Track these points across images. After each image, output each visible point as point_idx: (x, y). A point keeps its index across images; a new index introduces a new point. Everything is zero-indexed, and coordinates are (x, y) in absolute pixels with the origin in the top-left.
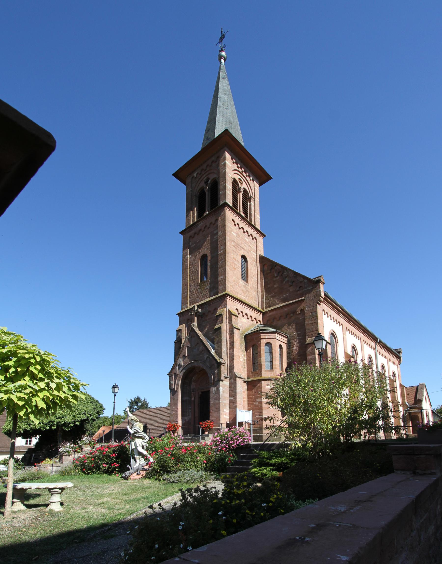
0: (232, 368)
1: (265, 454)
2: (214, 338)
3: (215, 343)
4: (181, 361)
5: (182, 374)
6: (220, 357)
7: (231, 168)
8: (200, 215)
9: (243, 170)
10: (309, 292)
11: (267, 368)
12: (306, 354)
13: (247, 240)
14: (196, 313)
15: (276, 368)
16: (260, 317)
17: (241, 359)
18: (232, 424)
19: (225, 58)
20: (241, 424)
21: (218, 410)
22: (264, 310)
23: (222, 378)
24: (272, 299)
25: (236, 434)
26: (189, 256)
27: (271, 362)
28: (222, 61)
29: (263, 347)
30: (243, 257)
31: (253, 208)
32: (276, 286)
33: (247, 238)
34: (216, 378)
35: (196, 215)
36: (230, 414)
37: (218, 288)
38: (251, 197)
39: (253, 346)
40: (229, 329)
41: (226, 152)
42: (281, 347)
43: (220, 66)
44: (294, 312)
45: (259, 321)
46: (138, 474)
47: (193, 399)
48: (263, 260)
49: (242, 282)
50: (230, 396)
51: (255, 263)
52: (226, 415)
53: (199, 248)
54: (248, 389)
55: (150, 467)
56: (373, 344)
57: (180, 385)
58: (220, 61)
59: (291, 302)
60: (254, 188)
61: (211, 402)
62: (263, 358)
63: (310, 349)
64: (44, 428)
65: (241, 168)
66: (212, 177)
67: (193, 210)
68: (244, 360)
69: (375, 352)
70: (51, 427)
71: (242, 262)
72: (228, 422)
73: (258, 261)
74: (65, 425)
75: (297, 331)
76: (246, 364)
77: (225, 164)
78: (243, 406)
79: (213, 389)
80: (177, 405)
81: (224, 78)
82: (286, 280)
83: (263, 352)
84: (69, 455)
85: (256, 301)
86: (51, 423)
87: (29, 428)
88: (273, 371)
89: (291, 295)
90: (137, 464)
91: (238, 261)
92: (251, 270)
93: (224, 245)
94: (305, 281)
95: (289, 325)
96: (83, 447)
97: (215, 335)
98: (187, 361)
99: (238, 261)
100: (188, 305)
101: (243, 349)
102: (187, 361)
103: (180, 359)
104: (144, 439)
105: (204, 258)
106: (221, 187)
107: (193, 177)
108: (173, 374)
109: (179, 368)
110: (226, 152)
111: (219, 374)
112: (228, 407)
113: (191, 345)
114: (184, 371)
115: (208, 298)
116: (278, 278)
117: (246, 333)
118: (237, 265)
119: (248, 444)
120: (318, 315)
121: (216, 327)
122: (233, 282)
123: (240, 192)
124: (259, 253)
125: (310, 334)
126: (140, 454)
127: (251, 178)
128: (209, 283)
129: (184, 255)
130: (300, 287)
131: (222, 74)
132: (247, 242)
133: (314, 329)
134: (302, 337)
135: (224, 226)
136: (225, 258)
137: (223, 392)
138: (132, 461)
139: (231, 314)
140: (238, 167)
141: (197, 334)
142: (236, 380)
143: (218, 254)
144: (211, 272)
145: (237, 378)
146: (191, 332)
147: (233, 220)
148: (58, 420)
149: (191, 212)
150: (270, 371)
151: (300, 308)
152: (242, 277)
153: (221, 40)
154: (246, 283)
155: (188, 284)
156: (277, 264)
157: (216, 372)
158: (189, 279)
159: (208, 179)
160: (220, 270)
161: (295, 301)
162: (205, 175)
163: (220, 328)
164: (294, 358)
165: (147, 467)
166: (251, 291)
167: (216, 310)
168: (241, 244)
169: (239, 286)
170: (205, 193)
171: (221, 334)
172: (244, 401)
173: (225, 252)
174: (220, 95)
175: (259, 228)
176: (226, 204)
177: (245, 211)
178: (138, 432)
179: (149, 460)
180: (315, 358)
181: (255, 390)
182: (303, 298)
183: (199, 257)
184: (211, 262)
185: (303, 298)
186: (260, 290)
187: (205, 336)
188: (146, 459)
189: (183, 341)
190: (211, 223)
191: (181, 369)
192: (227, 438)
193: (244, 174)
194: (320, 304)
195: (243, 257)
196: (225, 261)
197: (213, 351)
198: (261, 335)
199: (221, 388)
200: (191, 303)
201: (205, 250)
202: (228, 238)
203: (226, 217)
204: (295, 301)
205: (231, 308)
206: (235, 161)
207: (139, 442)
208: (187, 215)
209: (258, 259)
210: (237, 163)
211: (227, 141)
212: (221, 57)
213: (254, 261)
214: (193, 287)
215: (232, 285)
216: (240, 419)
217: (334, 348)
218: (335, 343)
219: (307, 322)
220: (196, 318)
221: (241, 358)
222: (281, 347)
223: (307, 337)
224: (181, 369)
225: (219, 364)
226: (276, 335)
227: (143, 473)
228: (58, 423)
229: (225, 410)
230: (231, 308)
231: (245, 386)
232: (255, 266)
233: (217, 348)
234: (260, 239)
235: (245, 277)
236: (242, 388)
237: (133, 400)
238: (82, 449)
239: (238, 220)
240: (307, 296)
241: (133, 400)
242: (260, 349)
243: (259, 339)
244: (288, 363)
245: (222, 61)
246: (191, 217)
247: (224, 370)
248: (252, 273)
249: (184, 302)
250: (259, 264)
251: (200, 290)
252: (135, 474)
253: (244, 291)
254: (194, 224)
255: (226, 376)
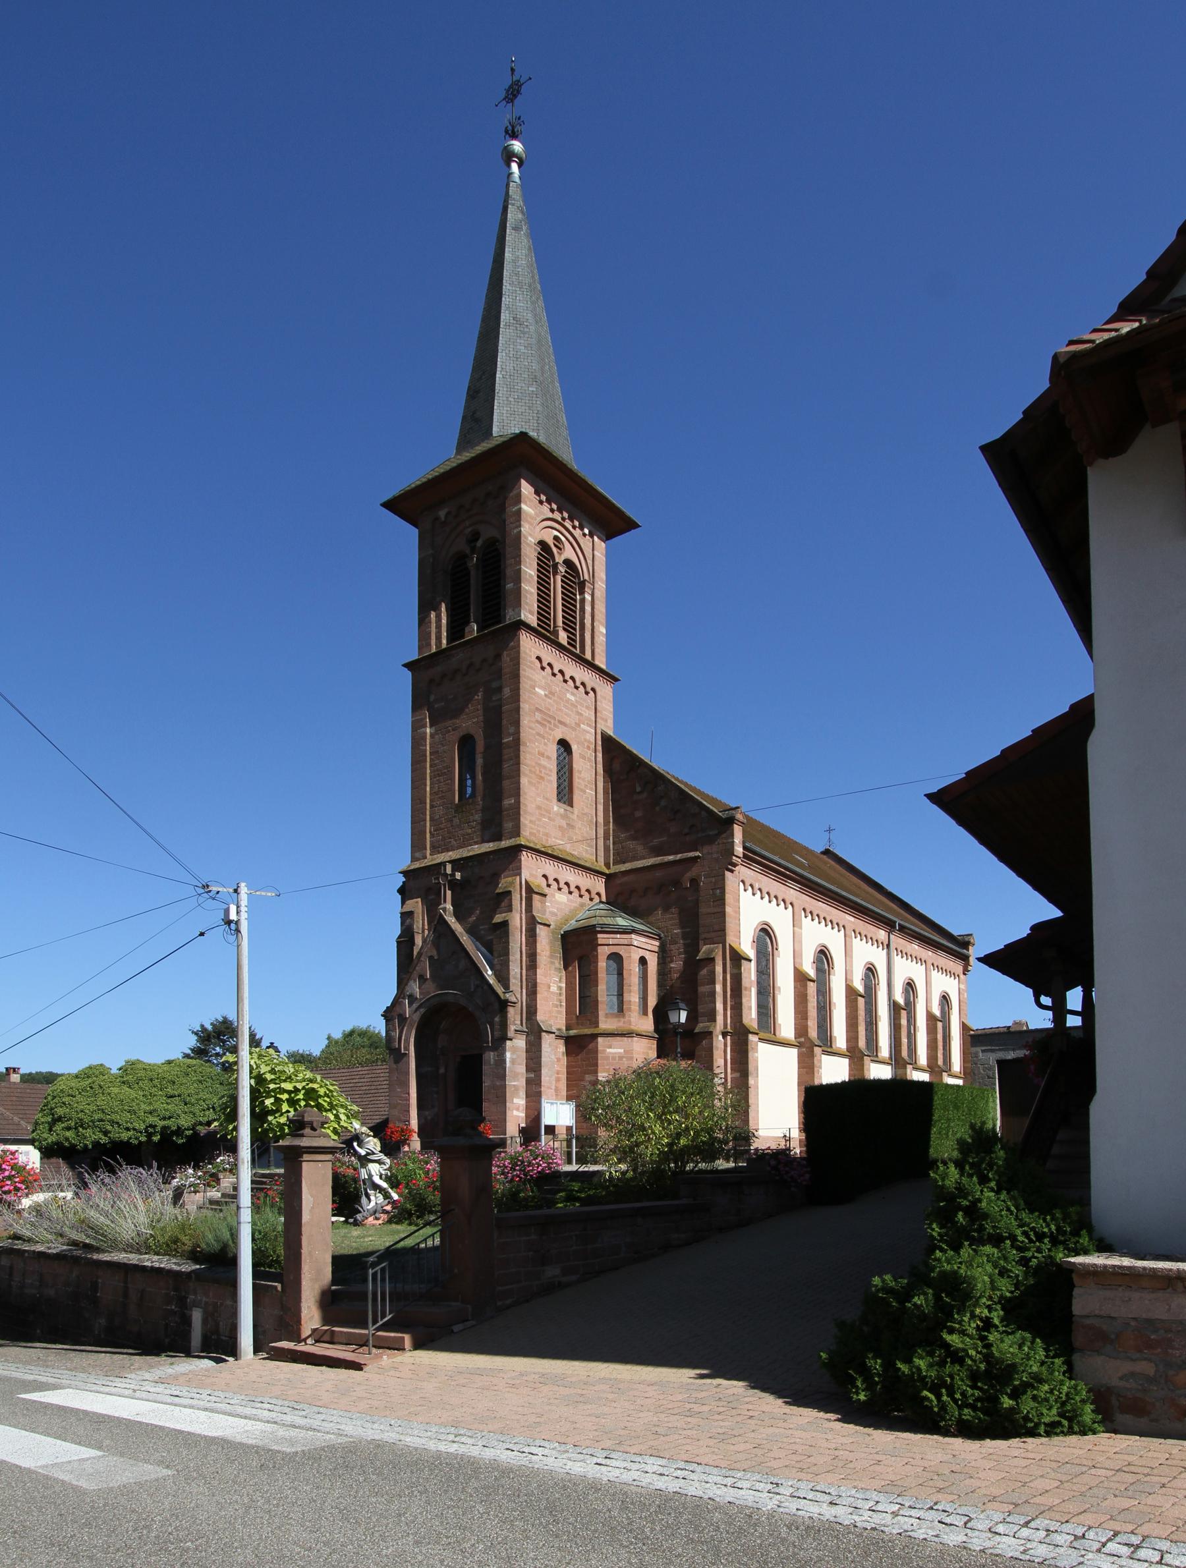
0: (531, 1011)
1: (576, 1186)
2: (491, 941)
3: (496, 954)
4: (415, 988)
5: (417, 1017)
6: (506, 987)
7: (535, 517)
8: (456, 629)
9: (566, 515)
10: (711, 840)
11: (611, 1008)
12: (696, 980)
13: (573, 698)
14: (450, 882)
15: (629, 1010)
16: (599, 885)
17: (554, 988)
18: (531, 1132)
19: (520, 159)
20: (551, 1130)
21: (501, 1099)
22: (609, 868)
23: (511, 1034)
24: (631, 844)
25: (538, 1156)
26: (428, 730)
27: (620, 995)
28: (514, 167)
29: (602, 964)
30: (564, 744)
31: (588, 608)
32: (638, 814)
33: (573, 694)
34: (497, 1034)
35: (444, 621)
36: (527, 1108)
37: (500, 825)
38: (585, 581)
39: (580, 959)
40: (527, 924)
41: (523, 482)
42: (643, 961)
43: (508, 185)
44: (677, 883)
45: (598, 894)
46: (377, 1219)
47: (442, 1071)
48: (611, 748)
49: (557, 808)
50: (528, 1070)
51: (591, 754)
52: (518, 1109)
53: (457, 712)
54: (568, 1053)
55: (393, 1208)
56: (882, 934)
57: (412, 1040)
58: (509, 166)
59: (671, 858)
60: (593, 553)
61: (487, 1083)
62: (602, 988)
63: (704, 972)
64: (137, 1138)
65: (560, 510)
66: (487, 532)
67: (437, 609)
68: (560, 988)
69: (889, 954)
70: (150, 1135)
71: (559, 756)
72: (523, 1125)
73: (599, 748)
74: (179, 1131)
75: (682, 927)
76: (563, 998)
77: (520, 510)
78: (557, 1090)
79: (490, 1056)
80: (406, 1085)
81: (516, 229)
82: (663, 803)
83: (602, 975)
84: (195, 1192)
85: (591, 847)
86: (151, 1130)
87: (104, 1140)
88: (624, 1016)
89: (671, 843)
90: (373, 1204)
91: (549, 758)
92: (580, 772)
93: (517, 723)
94: (703, 813)
95: (666, 909)
96: (221, 1176)
97: (495, 939)
98: (432, 990)
99: (549, 758)
100: (428, 852)
101: (559, 963)
102: (432, 990)
103: (411, 983)
104: (384, 1163)
105: (466, 742)
106: (509, 572)
107: (437, 519)
108: (395, 1014)
109: (410, 1004)
110: (523, 482)
111: (504, 1025)
112: (522, 1094)
113: (439, 954)
114: (422, 1010)
115: (476, 843)
116: (645, 795)
117: (567, 928)
118: (545, 767)
119: (558, 1172)
120: (727, 896)
121: (498, 918)
122: (540, 813)
123: (555, 573)
124: (601, 726)
125: (707, 935)
126: (376, 1187)
127: (586, 531)
128: (479, 807)
129: (417, 726)
130: (692, 826)
131: (513, 215)
132: (572, 705)
133: (716, 927)
134: (692, 947)
135: (516, 676)
136: (518, 757)
137: (513, 1062)
138: (364, 1200)
139: (530, 891)
140: (552, 511)
141: (452, 932)
142: (540, 1038)
143: (501, 744)
144: (484, 780)
145: (543, 1034)
146: (439, 925)
147: (538, 658)
148: (163, 1123)
149: (433, 615)
150: (617, 1016)
151: (689, 875)
152: (559, 793)
153: (513, 93)
154: (569, 808)
155: (428, 801)
156: (642, 763)
157: (497, 1019)
158: (428, 789)
159: (476, 536)
160: (506, 783)
161: (679, 856)
162: (467, 523)
163: (505, 924)
164: (672, 986)
165: (389, 1208)
166: (579, 824)
167: (495, 877)
168: (560, 708)
169: (550, 819)
170: (469, 574)
171: (508, 936)
172: (558, 1080)
173: (517, 743)
174: (506, 286)
175: (603, 667)
176: (521, 625)
177: (569, 626)
178: (374, 1153)
179: (391, 1197)
180: (714, 992)
181: (583, 1055)
182: (698, 854)
183: (454, 737)
184: (484, 758)
185: (698, 854)
186: (601, 820)
187: (471, 931)
188: (387, 1196)
189: (419, 941)
190: (484, 660)
191: (415, 1006)
192: (523, 1162)
193: (568, 524)
194: (732, 871)
195: (564, 744)
196: (519, 764)
197: (490, 972)
198: (599, 936)
199: (508, 1055)
200: (436, 849)
201: (471, 722)
202: (525, 707)
203: (522, 655)
204: (679, 856)
205: (532, 875)
206: (543, 498)
207: (374, 1168)
208: (423, 620)
209: (599, 742)
210: (549, 501)
211: (526, 457)
212: (509, 156)
213: (588, 748)
214: (440, 811)
215: (533, 819)
216: (548, 1119)
217: (768, 960)
218: (770, 949)
219: (703, 910)
220: (449, 893)
221: (553, 983)
222: (643, 961)
223: (701, 943)
224: (415, 1006)
225: (504, 1005)
226: (633, 936)
227: (384, 1217)
228: (164, 1128)
229: (515, 1100)
230: (532, 875)
231: (562, 1048)
232: (590, 760)
233: (498, 967)
234: (606, 691)
235: (565, 793)
236: (553, 1053)
237: (210, 1028)
238: (218, 1181)
239: (549, 654)
240: (706, 849)
241: (210, 1028)
242: (597, 967)
243: (595, 945)
244: (659, 995)
245: (514, 167)
246: (434, 625)
247: (515, 1018)
248: (583, 780)
249: (417, 845)
250: (600, 755)
251: (456, 821)
252: (371, 1219)
253: (562, 830)
254: (441, 653)
255: (519, 1028)
